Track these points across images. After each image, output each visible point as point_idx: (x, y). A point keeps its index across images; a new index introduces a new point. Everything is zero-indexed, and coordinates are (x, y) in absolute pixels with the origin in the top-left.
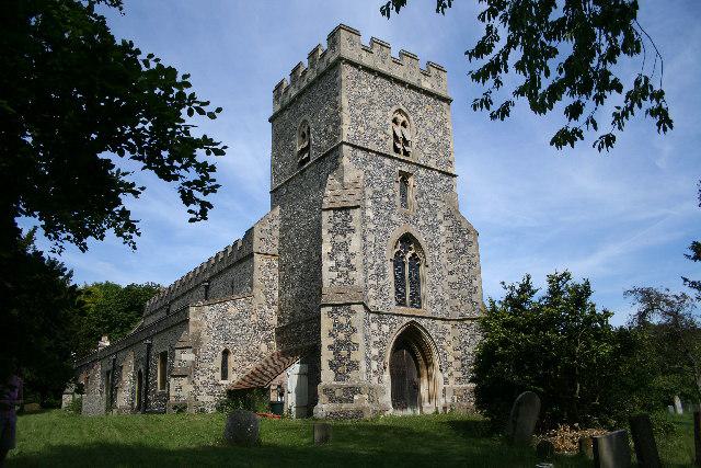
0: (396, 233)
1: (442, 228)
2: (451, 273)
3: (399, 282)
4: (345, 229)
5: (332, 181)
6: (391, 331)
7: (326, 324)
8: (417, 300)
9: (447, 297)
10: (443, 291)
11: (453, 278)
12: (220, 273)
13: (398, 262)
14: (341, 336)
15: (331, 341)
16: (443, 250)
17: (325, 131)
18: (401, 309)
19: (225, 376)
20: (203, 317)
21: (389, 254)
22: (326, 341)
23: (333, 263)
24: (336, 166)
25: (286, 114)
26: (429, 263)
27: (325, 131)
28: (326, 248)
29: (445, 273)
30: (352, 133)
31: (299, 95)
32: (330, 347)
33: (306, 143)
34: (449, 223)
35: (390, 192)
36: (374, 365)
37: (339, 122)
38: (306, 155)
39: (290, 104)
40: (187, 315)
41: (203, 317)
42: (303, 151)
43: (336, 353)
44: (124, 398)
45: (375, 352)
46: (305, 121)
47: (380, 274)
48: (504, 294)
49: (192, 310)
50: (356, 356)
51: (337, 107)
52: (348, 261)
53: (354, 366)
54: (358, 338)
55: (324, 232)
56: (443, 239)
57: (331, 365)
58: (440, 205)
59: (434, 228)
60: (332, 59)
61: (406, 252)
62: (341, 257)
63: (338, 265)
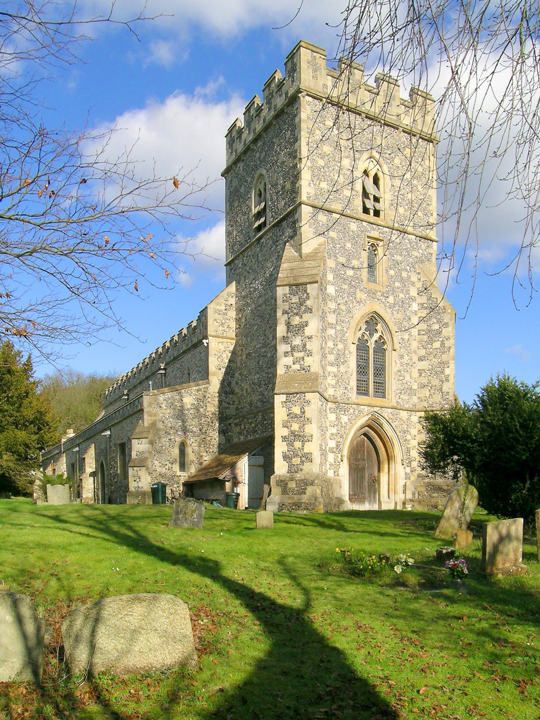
0: (360, 312)
1: (415, 307)
2: (421, 359)
3: (362, 370)
4: (301, 308)
5: (289, 251)
6: (354, 424)
7: (280, 414)
8: (380, 390)
9: (415, 386)
10: (412, 378)
11: (424, 365)
12: (175, 358)
13: (362, 346)
14: (295, 427)
15: (285, 432)
16: (414, 332)
17: (283, 187)
18: (363, 399)
19: (183, 466)
20: (157, 405)
21: (352, 338)
22: (280, 432)
23: (287, 307)
24: (295, 233)
25: (241, 165)
26: (397, 346)
27: (283, 187)
28: (281, 330)
29: (415, 358)
30: (312, 191)
31: (255, 141)
32: (284, 438)
33: (263, 204)
34: (423, 299)
35: (355, 263)
36: (331, 457)
37: (297, 177)
38: (262, 220)
39: (245, 152)
40: (142, 405)
41: (157, 405)
42: (259, 215)
43: (290, 444)
44: (89, 486)
45: (332, 444)
46: (261, 175)
47: (340, 360)
48: (424, 432)
49: (146, 400)
50: (312, 448)
51: (294, 155)
52: (304, 346)
53: (308, 458)
54: (311, 429)
55: (279, 313)
56: (415, 320)
57: (285, 457)
58: (414, 278)
59: (404, 304)
60: (291, 91)
61: (371, 335)
62: (297, 341)
63: (293, 349)
